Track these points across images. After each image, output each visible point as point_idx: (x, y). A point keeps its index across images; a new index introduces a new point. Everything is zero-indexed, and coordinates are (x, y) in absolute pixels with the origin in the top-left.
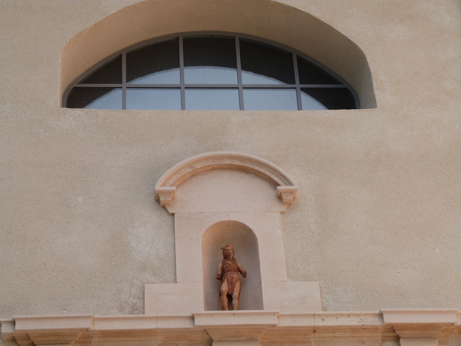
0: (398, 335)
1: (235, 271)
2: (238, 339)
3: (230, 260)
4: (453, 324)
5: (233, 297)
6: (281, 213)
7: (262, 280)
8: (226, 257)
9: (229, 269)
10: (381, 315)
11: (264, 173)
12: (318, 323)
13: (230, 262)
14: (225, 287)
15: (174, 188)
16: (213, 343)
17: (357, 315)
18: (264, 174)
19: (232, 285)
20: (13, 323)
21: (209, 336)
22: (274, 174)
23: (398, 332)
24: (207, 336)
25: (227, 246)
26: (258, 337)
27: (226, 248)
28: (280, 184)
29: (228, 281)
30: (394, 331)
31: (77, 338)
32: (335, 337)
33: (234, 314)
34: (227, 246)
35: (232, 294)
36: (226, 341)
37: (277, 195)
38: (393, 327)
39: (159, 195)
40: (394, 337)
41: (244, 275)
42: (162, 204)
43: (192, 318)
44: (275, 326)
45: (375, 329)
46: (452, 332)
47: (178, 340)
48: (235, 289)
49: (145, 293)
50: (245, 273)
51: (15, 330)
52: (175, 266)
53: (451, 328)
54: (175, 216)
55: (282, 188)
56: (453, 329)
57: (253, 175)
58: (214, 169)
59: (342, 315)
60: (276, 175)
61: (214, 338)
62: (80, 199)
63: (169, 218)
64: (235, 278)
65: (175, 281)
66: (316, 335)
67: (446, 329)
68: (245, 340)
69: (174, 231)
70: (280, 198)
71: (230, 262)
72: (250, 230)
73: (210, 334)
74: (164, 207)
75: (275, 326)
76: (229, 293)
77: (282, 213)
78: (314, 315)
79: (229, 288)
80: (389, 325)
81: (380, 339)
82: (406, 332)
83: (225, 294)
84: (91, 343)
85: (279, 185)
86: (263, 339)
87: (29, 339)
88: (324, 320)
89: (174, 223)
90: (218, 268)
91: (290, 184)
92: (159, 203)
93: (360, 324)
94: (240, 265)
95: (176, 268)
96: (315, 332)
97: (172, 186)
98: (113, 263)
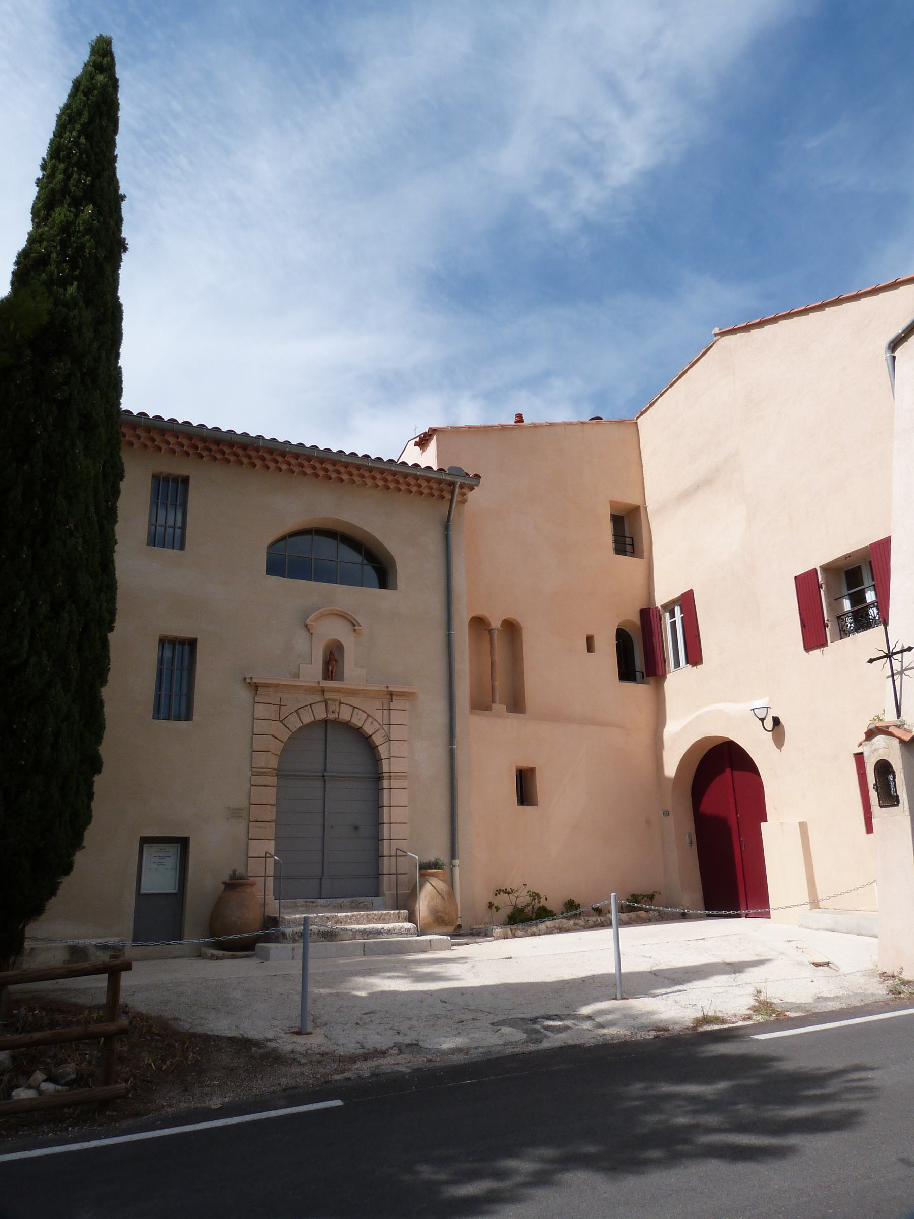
10: (388, 687)
74: (309, 630)
77: (355, 637)
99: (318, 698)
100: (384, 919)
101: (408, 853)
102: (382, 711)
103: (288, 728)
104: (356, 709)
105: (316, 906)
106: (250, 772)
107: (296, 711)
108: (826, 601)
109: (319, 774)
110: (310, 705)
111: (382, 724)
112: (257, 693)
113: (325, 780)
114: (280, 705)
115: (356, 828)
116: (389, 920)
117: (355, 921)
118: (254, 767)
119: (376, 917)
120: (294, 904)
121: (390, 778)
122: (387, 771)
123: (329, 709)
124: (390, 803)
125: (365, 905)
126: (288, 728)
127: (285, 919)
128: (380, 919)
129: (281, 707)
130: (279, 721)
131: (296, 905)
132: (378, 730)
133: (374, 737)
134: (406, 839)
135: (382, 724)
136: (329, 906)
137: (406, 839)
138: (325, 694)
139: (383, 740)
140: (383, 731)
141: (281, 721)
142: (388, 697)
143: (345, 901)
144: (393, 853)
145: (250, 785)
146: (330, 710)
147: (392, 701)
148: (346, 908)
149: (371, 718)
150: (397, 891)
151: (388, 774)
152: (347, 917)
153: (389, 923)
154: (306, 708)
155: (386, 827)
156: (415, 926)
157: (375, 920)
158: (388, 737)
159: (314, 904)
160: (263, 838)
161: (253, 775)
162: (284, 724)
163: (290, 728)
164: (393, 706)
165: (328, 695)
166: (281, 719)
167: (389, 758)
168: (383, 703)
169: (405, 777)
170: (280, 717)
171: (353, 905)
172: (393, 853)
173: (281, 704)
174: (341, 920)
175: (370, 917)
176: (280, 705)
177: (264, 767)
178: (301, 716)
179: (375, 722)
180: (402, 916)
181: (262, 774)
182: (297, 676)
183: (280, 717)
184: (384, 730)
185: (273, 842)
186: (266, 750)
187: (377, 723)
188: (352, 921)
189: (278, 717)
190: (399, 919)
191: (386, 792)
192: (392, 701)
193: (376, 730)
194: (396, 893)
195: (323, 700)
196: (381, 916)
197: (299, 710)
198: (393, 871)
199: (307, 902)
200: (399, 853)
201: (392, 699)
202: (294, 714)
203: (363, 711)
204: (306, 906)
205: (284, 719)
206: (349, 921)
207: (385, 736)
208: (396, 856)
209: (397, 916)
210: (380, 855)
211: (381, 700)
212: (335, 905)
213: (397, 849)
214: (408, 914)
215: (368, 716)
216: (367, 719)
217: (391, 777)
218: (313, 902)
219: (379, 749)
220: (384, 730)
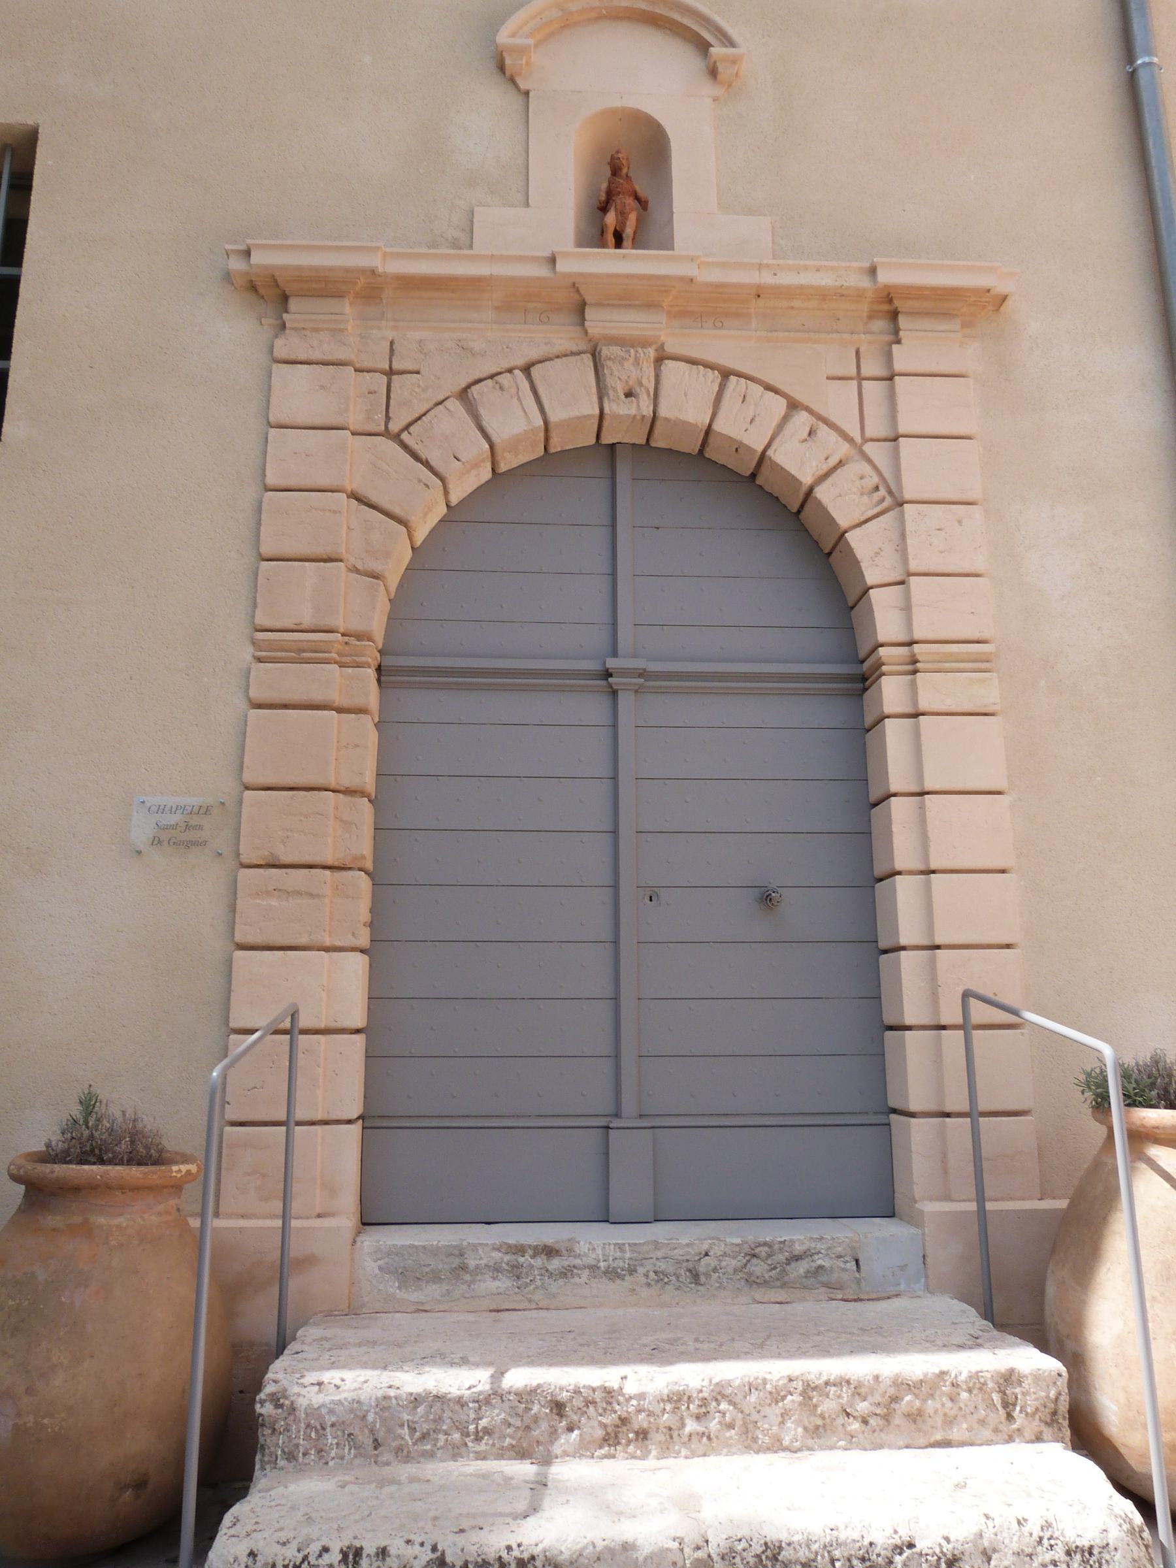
0: (897, 308)
1: (630, 196)
2: (628, 303)
3: (622, 179)
4: (989, 291)
5: (624, 236)
6: (714, 100)
7: (674, 210)
8: (615, 170)
9: (619, 190)
10: (873, 271)
11: (689, 25)
12: (767, 278)
13: (621, 181)
14: (611, 218)
15: (531, 41)
16: (586, 311)
17: (832, 269)
18: (688, 27)
19: (622, 215)
20: (247, 253)
21: (580, 295)
22: (706, 27)
23: (615, 687)
24: (577, 296)
25: (618, 152)
26: (663, 301)
27: (616, 156)
28: (712, 43)
29: (616, 210)
30: (890, 301)
31: (357, 288)
32: (792, 308)
33: (624, 257)
34: (618, 152)
35: (623, 231)
36: (609, 305)
37: (707, 68)
38: (889, 294)
39: (504, 53)
40: (889, 312)
41: (643, 203)
42: (507, 74)
43: (553, 260)
44: (692, 280)
45: (860, 295)
46: (984, 307)
47: (529, 302)
48: (628, 223)
49: (475, 221)
50: (647, 202)
51: (251, 266)
52: (528, 179)
53: (984, 299)
54: (531, 94)
55: (717, 51)
56: (986, 302)
57: (669, 32)
58: (600, 18)
59: (806, 268)
60: (710, 32)
61: (588, 299)
62: (367, 59)
63: (519, 100)
64: (629, 204)
65: (527, 204)
66: (761, 302)
67: (975, 301)
68: (639, 306)
69: (527, 122)
70: (713, 73)
71: (621, 181)
72: (659, 126)
73: (582, 292)
74: (512, 81)
75: (692, 280)
76: (618, 228)
77: (715, 100)
78: (760, 267)
79: (617, 220)
80: (886, 286)
81: (865, 314)
82: (910, 303)
83: (611, 230)
84: (381, 299)
85: (713, 46)
86: (671, 306)
87: (277, 286)
88: (775, 274)
89: (528, 108)
90: (600, 190)
91: (732, 44)
92: (504, 73)
93: (838, 284)
94: (638, 188)
95: (528, 183)
96: (759, 296)
97: (527, 37)
98: (421, 171)
99: (562, 337)
100: (915, 1417)
101: (1030, 1016)
102: (855, 383)
103: (426, 464)
104: (733, 379)
105: (566, 1273)
106: (250, 649)
107: (463, 394)
108: (206, 1344)
109: (593, 665)
110: (527, 369)
111: (858, 440)
112: (283, 326)
113: (614, 693)
114: (390, 373)
115: (767, 899)
116: (949, 1422)
117: (731, 1426)
118: (268, 623)
119: (863, 1407)
120: (456, 1262)
121: (913, 667)
122: (894, 639)
123: (610, 381)
124: (920, 776)
125: (821, 1267)
126: (426, 464)
127: (293, 1409)
128: (887, 1418)
129: (395, 377)
130: (386, 434)
131: (463, 1268)
132: (840, 464)
133: (823, 493)
134: (1008, 946)
135: (858, 440)
136: (632, 1271)
137: (1008, 946)
138: (587, 316)
139: (864, 506)
140: (865, 468)
141: (397, 438)
142: (880, 325)
143: (718, 1250)
144: (951, 1013)
145: (242, 704)
146: (616, 382)
147: (899, 342)
148: (721, 1287)
149: (804, 415)
150: (981, 1199)
151: (903, 651)
152: (677, 1399)
153: (946, 1444)
154: (505, 379)
155: (905, 890)
156: (1138, 1519)
157: (855, 1426)
158: (890, 492)
159: (555, 1264)
160: (304, 940)
161: (260, 660)
162: (405, 447)
163: (433, 463)
164: (903, 358)
165: (599, 322)
166: (394, 427)
167: (902, 583)
168: (858, 353)
169: (982, 664)
170: (388, 418)
171: (759, 1268)
172: (951, 1013)
173: (396, 366)
174: (641, 1420)
175: (828, 1406)
176: (390, 373)
177: (307, 622)
178: (482, 411)
179: (823, 430)
180: (1031, 1398)
181: (300, 656)
182: (465, 240)
183: (388, 418)
184: (869, 461)
185: (357, 965)
186: (320, 551)
187: (833, 437)
188: (714, 1425)
189: (381, 416)
190: (1010, 1417)
191: (894, 733)
192: (899, 342)
193: (833, 461)
194: (982, 1212)
195: (583, 346)
196: (895, 1399)
197: (474, 389)
198: (957, 1101)
199: (520, 1250)
200: (980, 1012)
201: (896, 331)
202: (454, 405)
203: (769, 388)
204: (516, 1272)
205: (407, 428)
206: (691, 1426)
207: (877, 488)
208: (965, 1027)
209: (996, 1397)
210: (889, 1019)
211: (846, 336)
212: (662, 1266)
213: (966, 995)
214: (1062, 1383)
215: (794, 406)
216: (786, 419)
217: (916, 662)
218: (549, 1252)
219: (853, 544)
220: (869, 461)
